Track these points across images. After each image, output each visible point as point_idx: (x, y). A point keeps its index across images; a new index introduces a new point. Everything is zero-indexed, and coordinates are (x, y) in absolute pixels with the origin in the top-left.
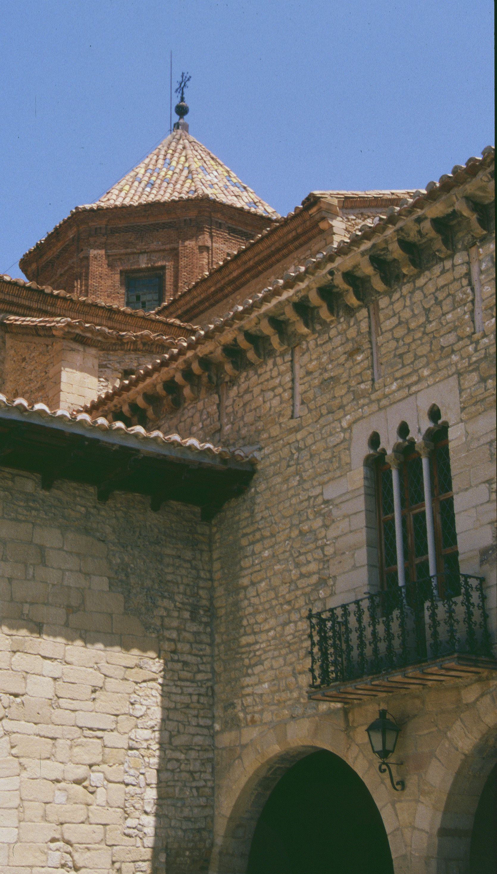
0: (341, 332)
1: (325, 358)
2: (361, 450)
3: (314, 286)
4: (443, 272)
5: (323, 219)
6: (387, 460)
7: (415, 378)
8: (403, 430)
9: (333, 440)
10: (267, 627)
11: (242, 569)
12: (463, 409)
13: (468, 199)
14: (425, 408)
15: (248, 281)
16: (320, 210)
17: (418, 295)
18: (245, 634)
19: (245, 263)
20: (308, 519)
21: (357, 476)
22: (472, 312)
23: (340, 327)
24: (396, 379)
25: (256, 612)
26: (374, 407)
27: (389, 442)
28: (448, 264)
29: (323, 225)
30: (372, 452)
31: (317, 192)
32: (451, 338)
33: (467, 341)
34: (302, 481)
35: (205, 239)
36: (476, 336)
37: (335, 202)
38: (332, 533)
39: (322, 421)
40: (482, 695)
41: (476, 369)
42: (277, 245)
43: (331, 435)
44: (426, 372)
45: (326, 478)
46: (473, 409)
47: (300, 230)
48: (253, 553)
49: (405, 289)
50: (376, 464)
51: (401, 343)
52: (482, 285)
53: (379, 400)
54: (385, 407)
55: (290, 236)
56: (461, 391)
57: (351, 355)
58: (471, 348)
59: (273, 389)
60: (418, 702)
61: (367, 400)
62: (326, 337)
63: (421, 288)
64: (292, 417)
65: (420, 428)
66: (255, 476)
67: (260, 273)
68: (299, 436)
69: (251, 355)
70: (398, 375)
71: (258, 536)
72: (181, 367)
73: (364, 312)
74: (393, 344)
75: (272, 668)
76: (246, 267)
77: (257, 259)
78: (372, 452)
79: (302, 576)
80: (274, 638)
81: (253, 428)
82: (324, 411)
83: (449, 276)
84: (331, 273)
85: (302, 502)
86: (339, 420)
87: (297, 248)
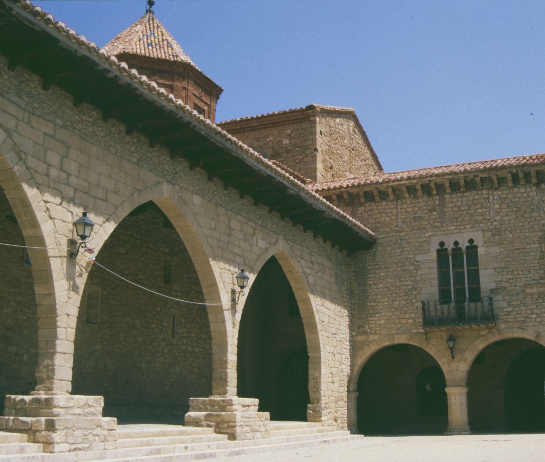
0: (423, 200)
1: (416, 209)
2: (435, 246)
3: (420, 183)
4: (477, 194)
5: (313, 116)
6: (448, 252)
7: (463, 227)
8: (456, 243)
9: (420, 240)
10: (383, 301)
11: (368, 278)
12: (485, 243)
13: (497, 176)
14: (467, 238)
15: (260, 129)
16: (313, 112)
17: (465, 199)
18: (370, 302)
19: (262, 121)
20: (406, 265)
21: (434, 255)
22: (489, 211)
23: (424, 199)
24: (454, 226)
25: (377, 295)
26: (442, 233)
27: (450, 246)
28: (480, 192)
29: (312, 118)
30: (440, 248)
31: (315, 105)
32: (480, 218)
33: (487, 221)
34: (403, 251)
35: (185, 84)
36: (491, 220)
37: (319, 110)
38: (419, 272)
39: (415, 231)
40: (489, 333)
41: (491, 231)
42: (284, 119)
43: (419, 237)
44: (468, 227)
45: (417, 252)
46: (489, 244)
47: (299, 117)
48: (375, 273)
49: (458, 195)
50: (442, 252)
51: (456, 213)
52: (494, 204)
53: (444, 231)
54: (448, 234)
55: (293, 118)
56: (484, 237)
57: (431, 211)
58: (489, 224)
59: (386, 213)
60: (461, 333)
61: (438, 229)
62: (417, 201)
63: (467, 197)
64: (397, 226)
65: (464, 244)
66: (376, 245)
67: (269, 127)
68: (401, 234)
69: (377, 198)
70: (455, 224)
71: (377, 267)
72: (337, 193)
73: (437, 197)
74: (452, 213)
75: (386, 315)
76: (263, 123)
77: (270, 122)
78: (440, 248)
79: (403, 285)
80: (387, 305)
81: (375, 225)
82: (416, 228)
83: (480, 197)
84: (430, 181)
85: (402, 259)
86: (425, 234)
87: (293, 123)
